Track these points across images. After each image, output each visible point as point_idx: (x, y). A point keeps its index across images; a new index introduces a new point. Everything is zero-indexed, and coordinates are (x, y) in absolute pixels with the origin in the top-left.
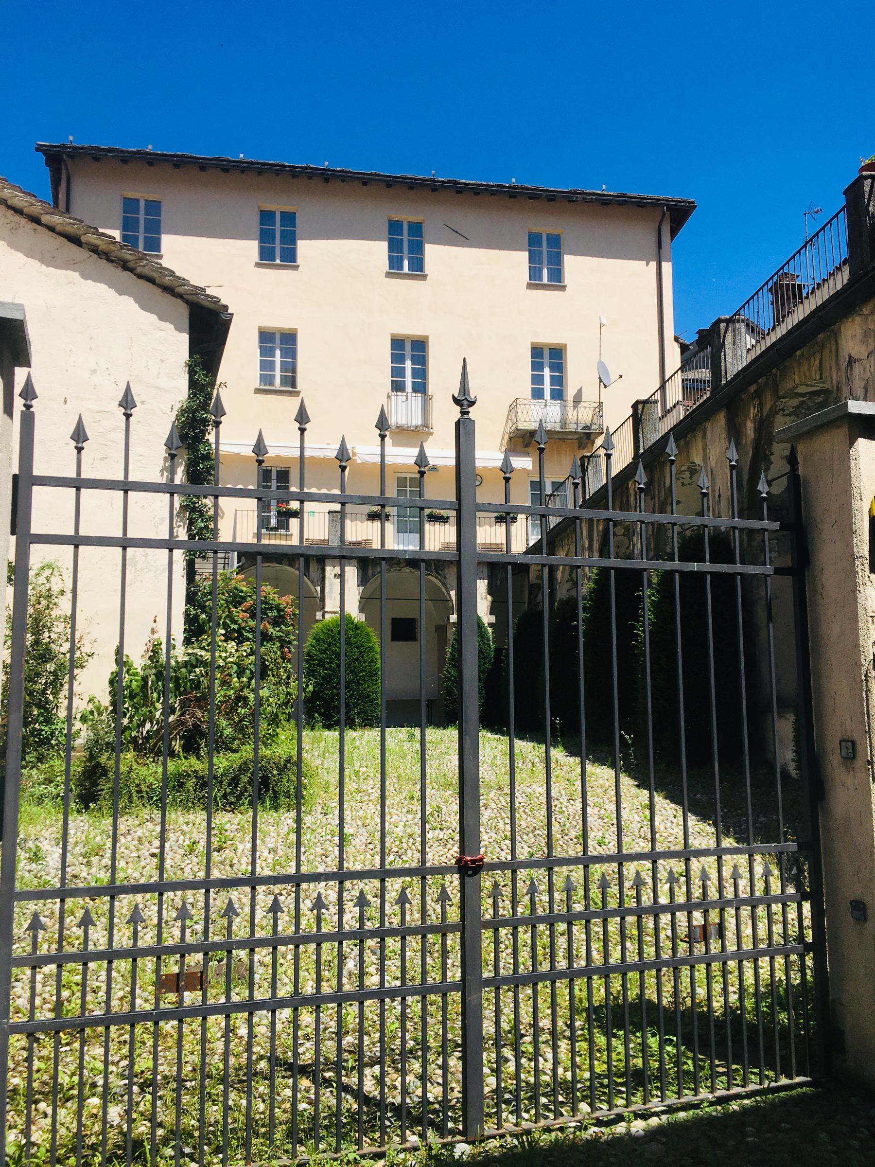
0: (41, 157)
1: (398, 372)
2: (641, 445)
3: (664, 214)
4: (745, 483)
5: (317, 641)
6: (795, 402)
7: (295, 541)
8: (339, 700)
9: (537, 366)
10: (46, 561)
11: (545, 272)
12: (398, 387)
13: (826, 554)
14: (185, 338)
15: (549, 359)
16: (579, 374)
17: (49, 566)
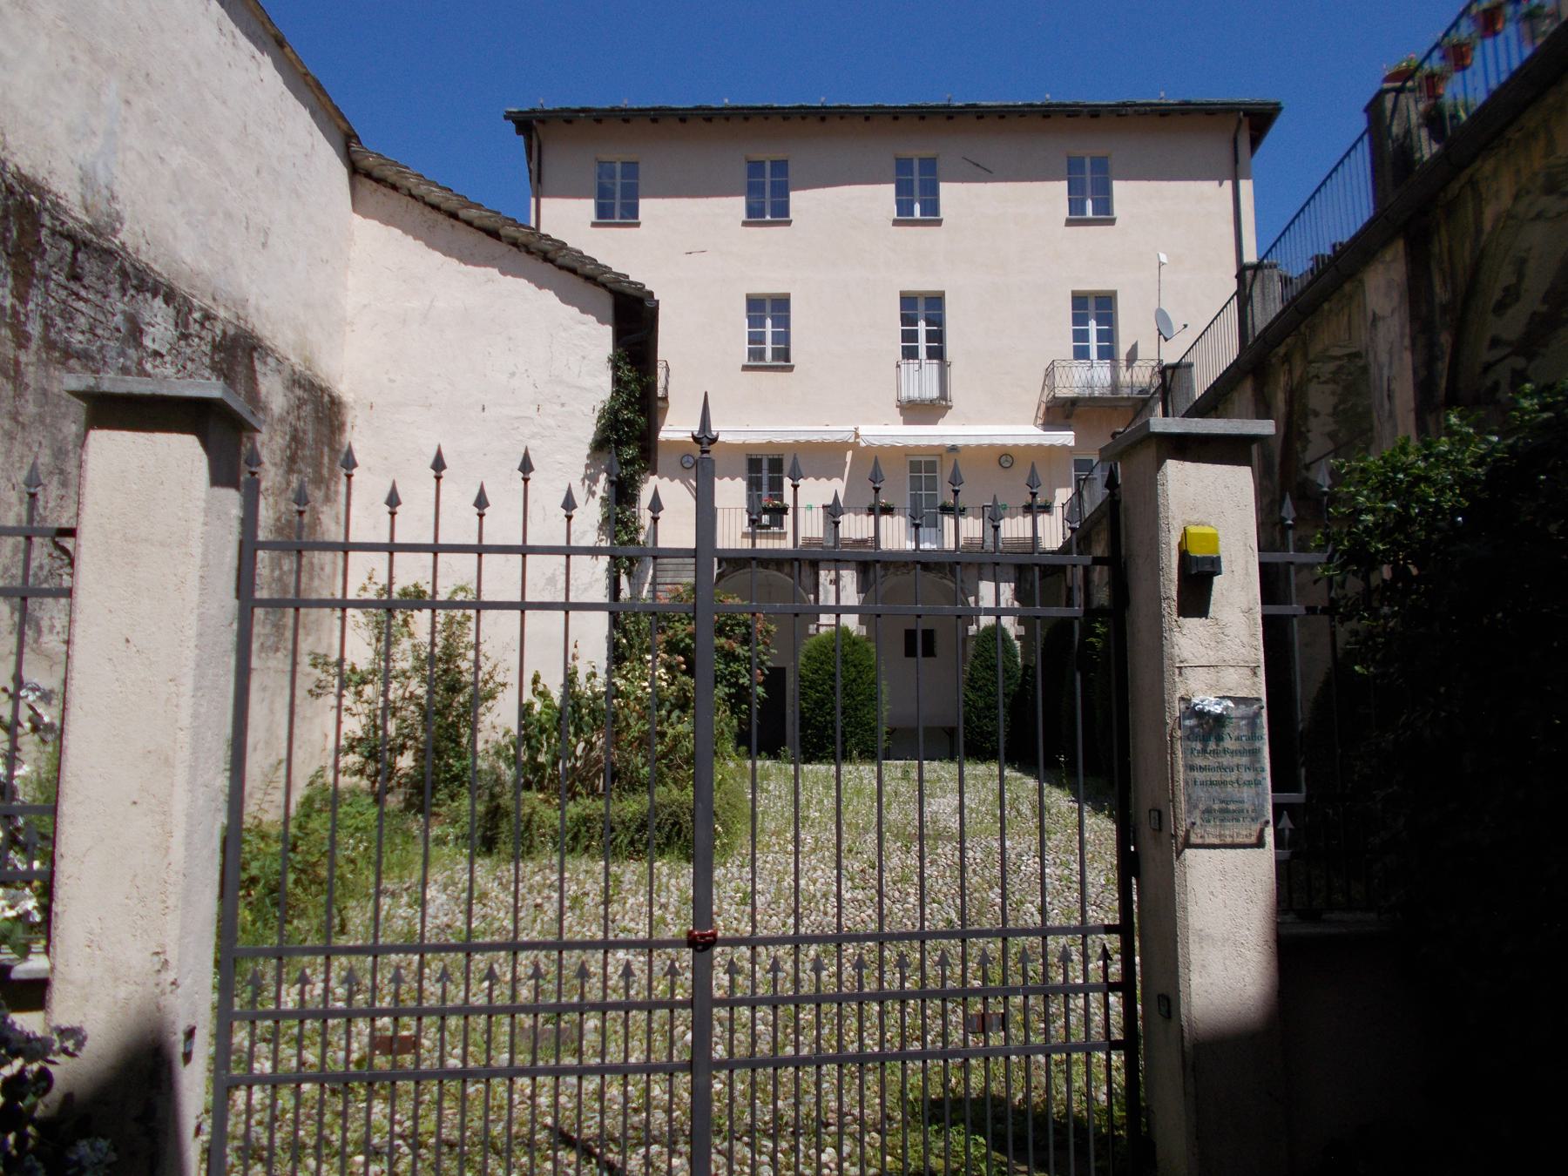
0: (511, 126)
1: (909, 336)
3: (1240, 121)
5: (809, 658)
6: (1332, 366)
7: (787, 544)
8: (834, 729)
10: (460, 583)
11: (1089, 204)
12: (910, 354)
13: (1139, 595)
14: (608, 330)
15: (1095, 308)
16: (1133, 327)
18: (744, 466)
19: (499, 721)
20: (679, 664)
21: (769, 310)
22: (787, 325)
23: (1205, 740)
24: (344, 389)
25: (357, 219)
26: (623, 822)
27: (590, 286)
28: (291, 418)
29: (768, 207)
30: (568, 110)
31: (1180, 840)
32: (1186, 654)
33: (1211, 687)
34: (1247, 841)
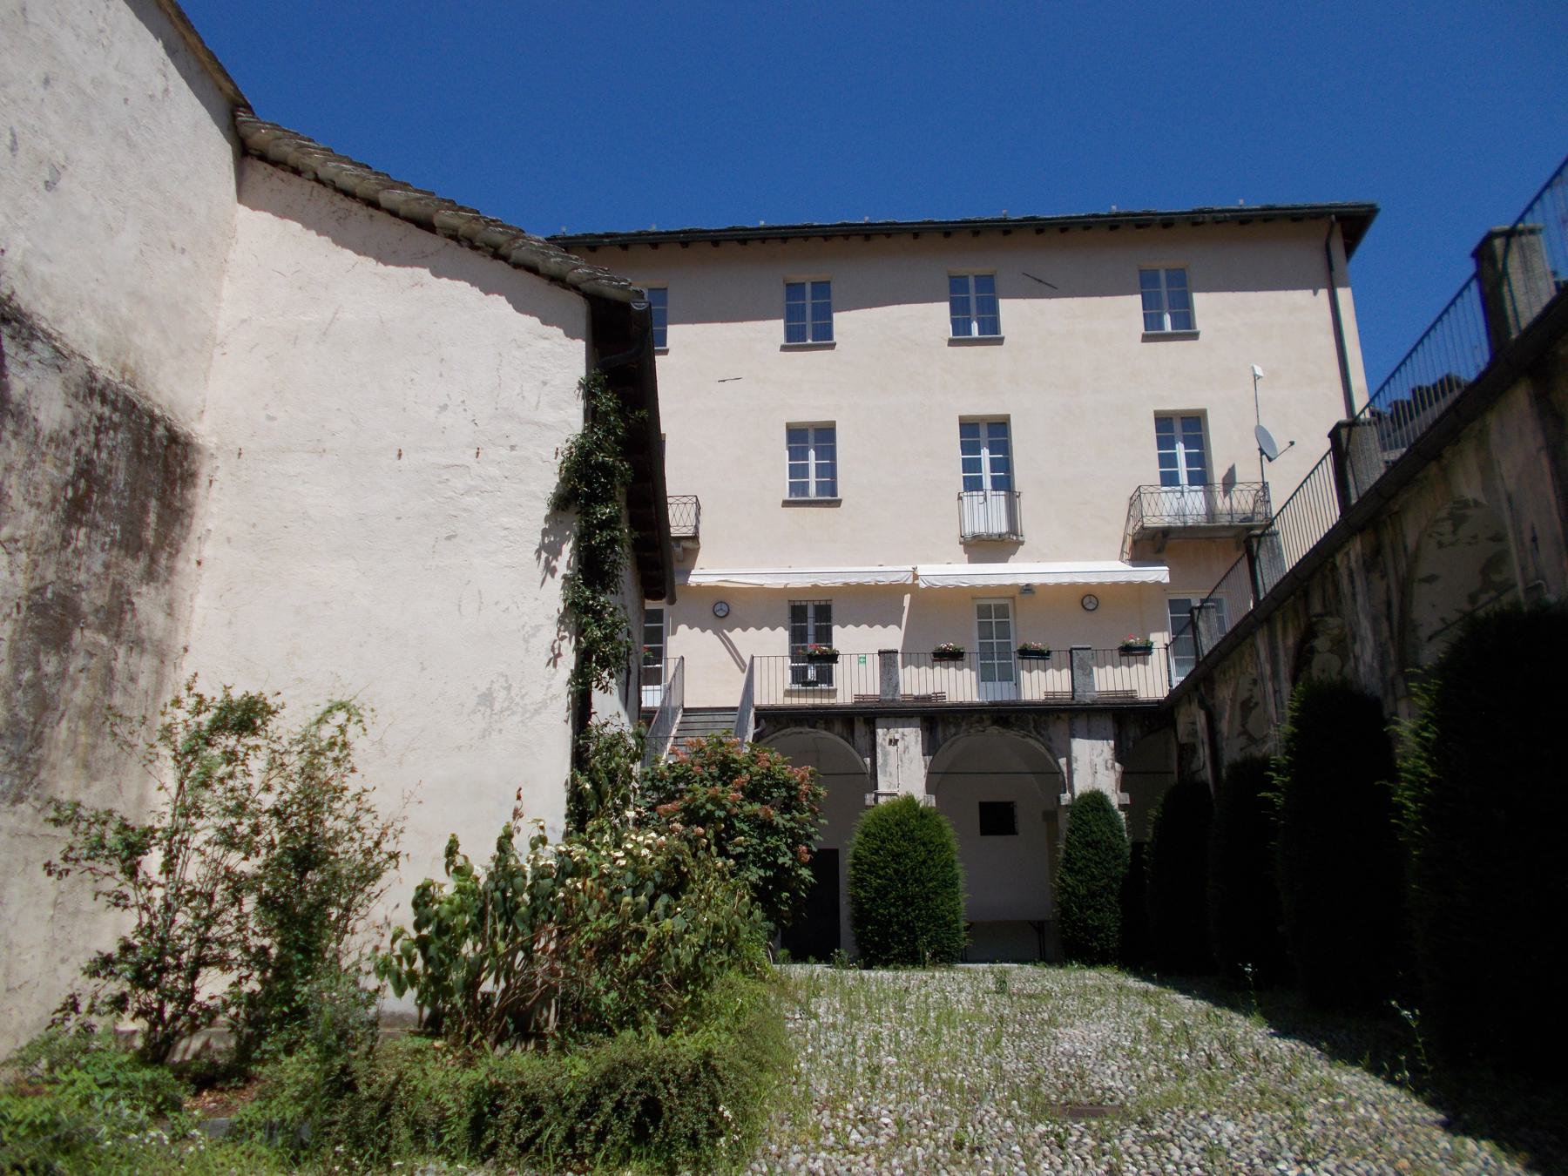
2: (1353, 491)
3: (1332, 225)
9: (1165, 441)
10: (337, 699)
12: (973, 484)
14: (580, 346)
15: (1182, 430)
16: (1228, 447)
17: (342, 706)
18: (786, 613)
19: (381, 920)
21: (812, 442)
22: (833, 456)
24: (203, 431)
25: (243, 211)
26: (558, 1098)
27: (556, 290)
28: (84, 442)
29: (809, 328)
30: (592, 236)
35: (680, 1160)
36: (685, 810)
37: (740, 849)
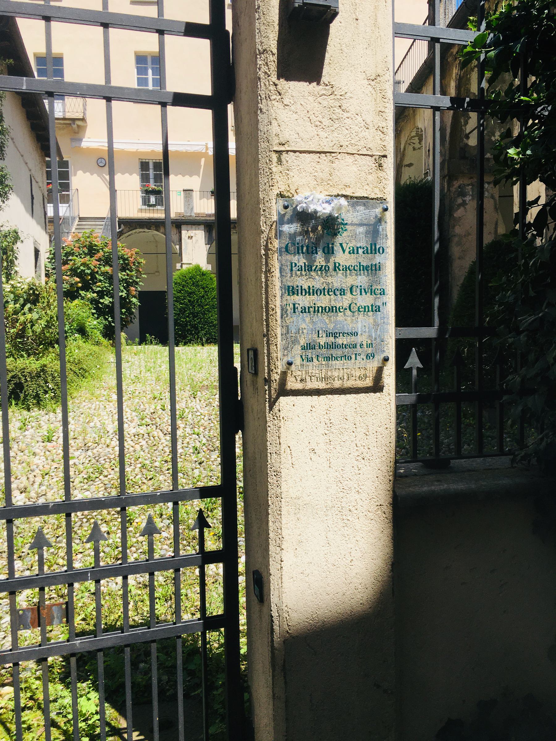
4: (447, 138)
18: (138, 166)
20: (77, 283)
23: (311, 252)
31: (275, 385)
32: (287, 134)
33: (320, 182)
34: (360, 384)
35: (31, 404)
36: (71, 270)
37: (99, 289)
